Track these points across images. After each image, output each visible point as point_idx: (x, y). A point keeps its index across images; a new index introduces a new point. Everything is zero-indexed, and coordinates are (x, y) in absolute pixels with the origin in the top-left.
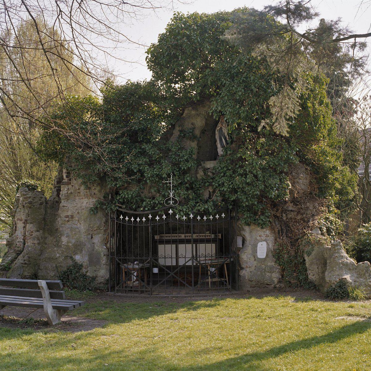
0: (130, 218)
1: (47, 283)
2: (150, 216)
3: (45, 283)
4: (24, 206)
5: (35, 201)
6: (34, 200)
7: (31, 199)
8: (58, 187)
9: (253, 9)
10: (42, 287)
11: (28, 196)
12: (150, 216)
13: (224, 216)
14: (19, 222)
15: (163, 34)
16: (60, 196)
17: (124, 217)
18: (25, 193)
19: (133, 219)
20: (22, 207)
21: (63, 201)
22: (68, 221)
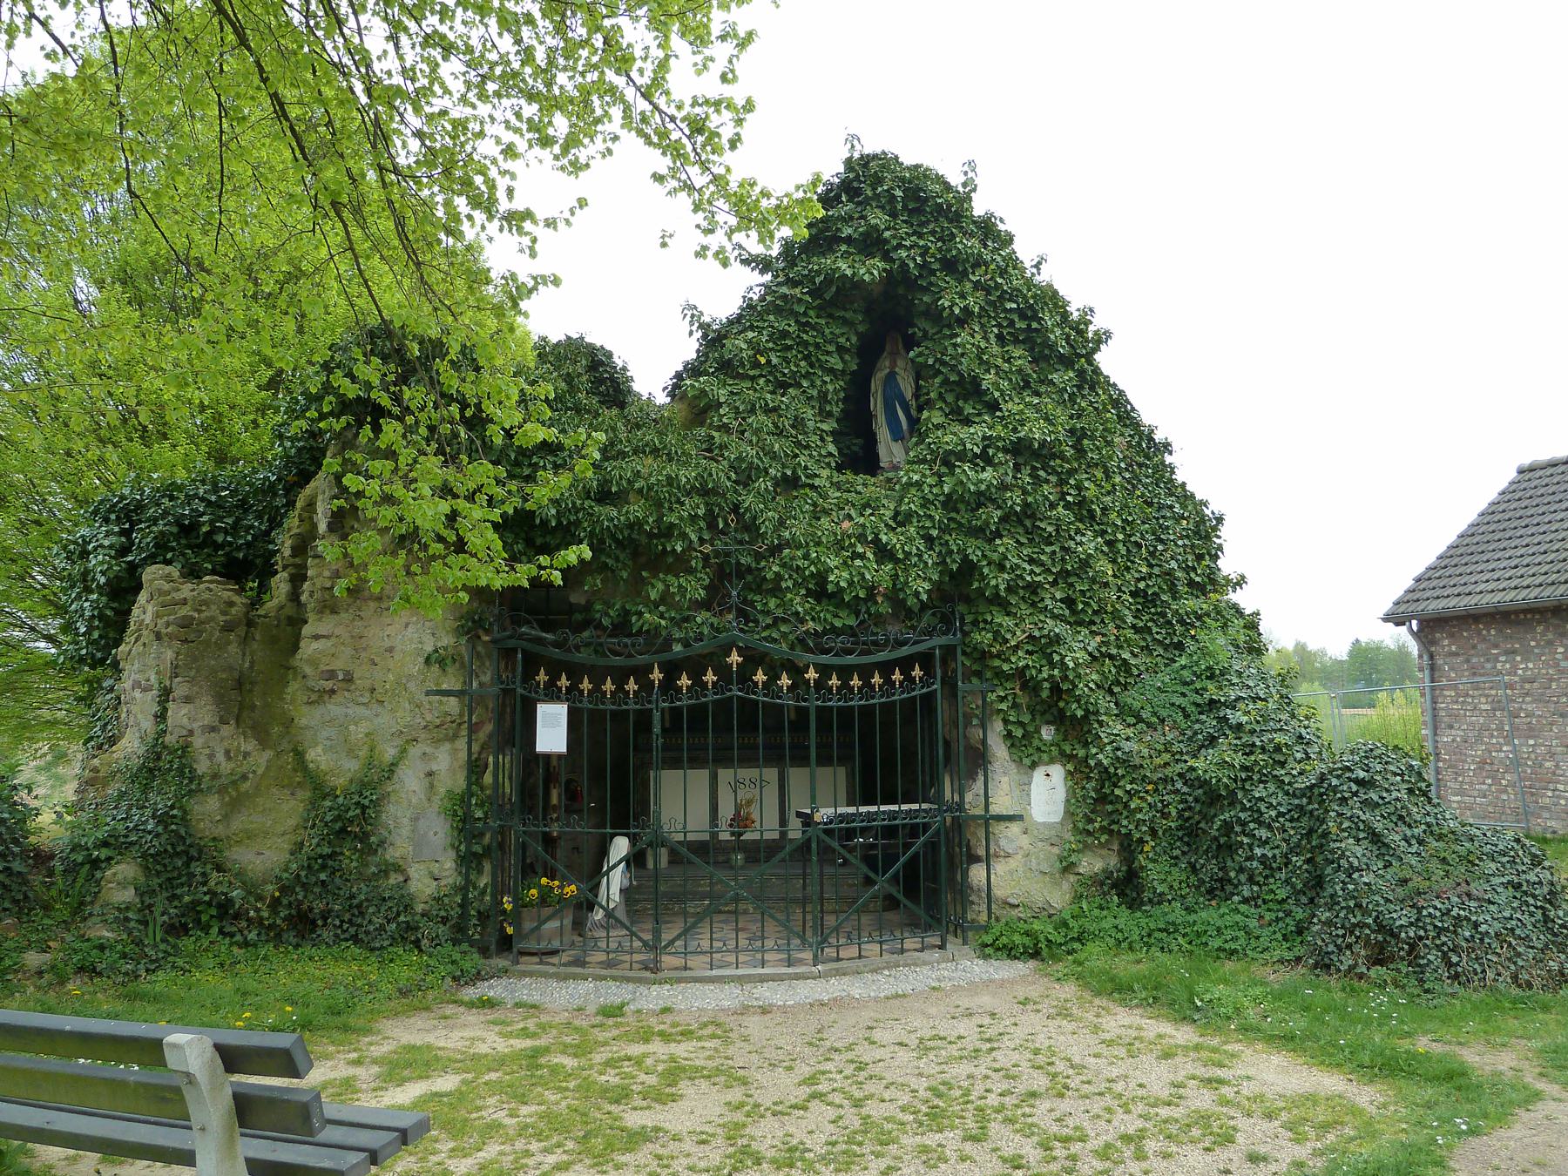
0: (597, 682)
1: (218, 1048)
2: (657, 675)
3: (210, 1051)
4: (158, 636)
5: (203, 615)
6: (200, 612)
7: (188, 607)
8: (295, 565)
9: (1301, 649)
10: (188, 1074)
11: (178, 596)
12: (657, 675)
13: (661, 676)
14: (137, 694)
15: (367, 51)
16: (303, 598)
17: (773, 677)
18: (167, 587)
19: (609, 686)
20: (152, 637)
21: (311, 617)
22: (333, 692)
